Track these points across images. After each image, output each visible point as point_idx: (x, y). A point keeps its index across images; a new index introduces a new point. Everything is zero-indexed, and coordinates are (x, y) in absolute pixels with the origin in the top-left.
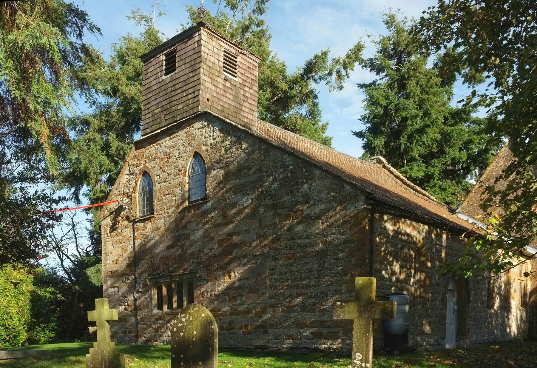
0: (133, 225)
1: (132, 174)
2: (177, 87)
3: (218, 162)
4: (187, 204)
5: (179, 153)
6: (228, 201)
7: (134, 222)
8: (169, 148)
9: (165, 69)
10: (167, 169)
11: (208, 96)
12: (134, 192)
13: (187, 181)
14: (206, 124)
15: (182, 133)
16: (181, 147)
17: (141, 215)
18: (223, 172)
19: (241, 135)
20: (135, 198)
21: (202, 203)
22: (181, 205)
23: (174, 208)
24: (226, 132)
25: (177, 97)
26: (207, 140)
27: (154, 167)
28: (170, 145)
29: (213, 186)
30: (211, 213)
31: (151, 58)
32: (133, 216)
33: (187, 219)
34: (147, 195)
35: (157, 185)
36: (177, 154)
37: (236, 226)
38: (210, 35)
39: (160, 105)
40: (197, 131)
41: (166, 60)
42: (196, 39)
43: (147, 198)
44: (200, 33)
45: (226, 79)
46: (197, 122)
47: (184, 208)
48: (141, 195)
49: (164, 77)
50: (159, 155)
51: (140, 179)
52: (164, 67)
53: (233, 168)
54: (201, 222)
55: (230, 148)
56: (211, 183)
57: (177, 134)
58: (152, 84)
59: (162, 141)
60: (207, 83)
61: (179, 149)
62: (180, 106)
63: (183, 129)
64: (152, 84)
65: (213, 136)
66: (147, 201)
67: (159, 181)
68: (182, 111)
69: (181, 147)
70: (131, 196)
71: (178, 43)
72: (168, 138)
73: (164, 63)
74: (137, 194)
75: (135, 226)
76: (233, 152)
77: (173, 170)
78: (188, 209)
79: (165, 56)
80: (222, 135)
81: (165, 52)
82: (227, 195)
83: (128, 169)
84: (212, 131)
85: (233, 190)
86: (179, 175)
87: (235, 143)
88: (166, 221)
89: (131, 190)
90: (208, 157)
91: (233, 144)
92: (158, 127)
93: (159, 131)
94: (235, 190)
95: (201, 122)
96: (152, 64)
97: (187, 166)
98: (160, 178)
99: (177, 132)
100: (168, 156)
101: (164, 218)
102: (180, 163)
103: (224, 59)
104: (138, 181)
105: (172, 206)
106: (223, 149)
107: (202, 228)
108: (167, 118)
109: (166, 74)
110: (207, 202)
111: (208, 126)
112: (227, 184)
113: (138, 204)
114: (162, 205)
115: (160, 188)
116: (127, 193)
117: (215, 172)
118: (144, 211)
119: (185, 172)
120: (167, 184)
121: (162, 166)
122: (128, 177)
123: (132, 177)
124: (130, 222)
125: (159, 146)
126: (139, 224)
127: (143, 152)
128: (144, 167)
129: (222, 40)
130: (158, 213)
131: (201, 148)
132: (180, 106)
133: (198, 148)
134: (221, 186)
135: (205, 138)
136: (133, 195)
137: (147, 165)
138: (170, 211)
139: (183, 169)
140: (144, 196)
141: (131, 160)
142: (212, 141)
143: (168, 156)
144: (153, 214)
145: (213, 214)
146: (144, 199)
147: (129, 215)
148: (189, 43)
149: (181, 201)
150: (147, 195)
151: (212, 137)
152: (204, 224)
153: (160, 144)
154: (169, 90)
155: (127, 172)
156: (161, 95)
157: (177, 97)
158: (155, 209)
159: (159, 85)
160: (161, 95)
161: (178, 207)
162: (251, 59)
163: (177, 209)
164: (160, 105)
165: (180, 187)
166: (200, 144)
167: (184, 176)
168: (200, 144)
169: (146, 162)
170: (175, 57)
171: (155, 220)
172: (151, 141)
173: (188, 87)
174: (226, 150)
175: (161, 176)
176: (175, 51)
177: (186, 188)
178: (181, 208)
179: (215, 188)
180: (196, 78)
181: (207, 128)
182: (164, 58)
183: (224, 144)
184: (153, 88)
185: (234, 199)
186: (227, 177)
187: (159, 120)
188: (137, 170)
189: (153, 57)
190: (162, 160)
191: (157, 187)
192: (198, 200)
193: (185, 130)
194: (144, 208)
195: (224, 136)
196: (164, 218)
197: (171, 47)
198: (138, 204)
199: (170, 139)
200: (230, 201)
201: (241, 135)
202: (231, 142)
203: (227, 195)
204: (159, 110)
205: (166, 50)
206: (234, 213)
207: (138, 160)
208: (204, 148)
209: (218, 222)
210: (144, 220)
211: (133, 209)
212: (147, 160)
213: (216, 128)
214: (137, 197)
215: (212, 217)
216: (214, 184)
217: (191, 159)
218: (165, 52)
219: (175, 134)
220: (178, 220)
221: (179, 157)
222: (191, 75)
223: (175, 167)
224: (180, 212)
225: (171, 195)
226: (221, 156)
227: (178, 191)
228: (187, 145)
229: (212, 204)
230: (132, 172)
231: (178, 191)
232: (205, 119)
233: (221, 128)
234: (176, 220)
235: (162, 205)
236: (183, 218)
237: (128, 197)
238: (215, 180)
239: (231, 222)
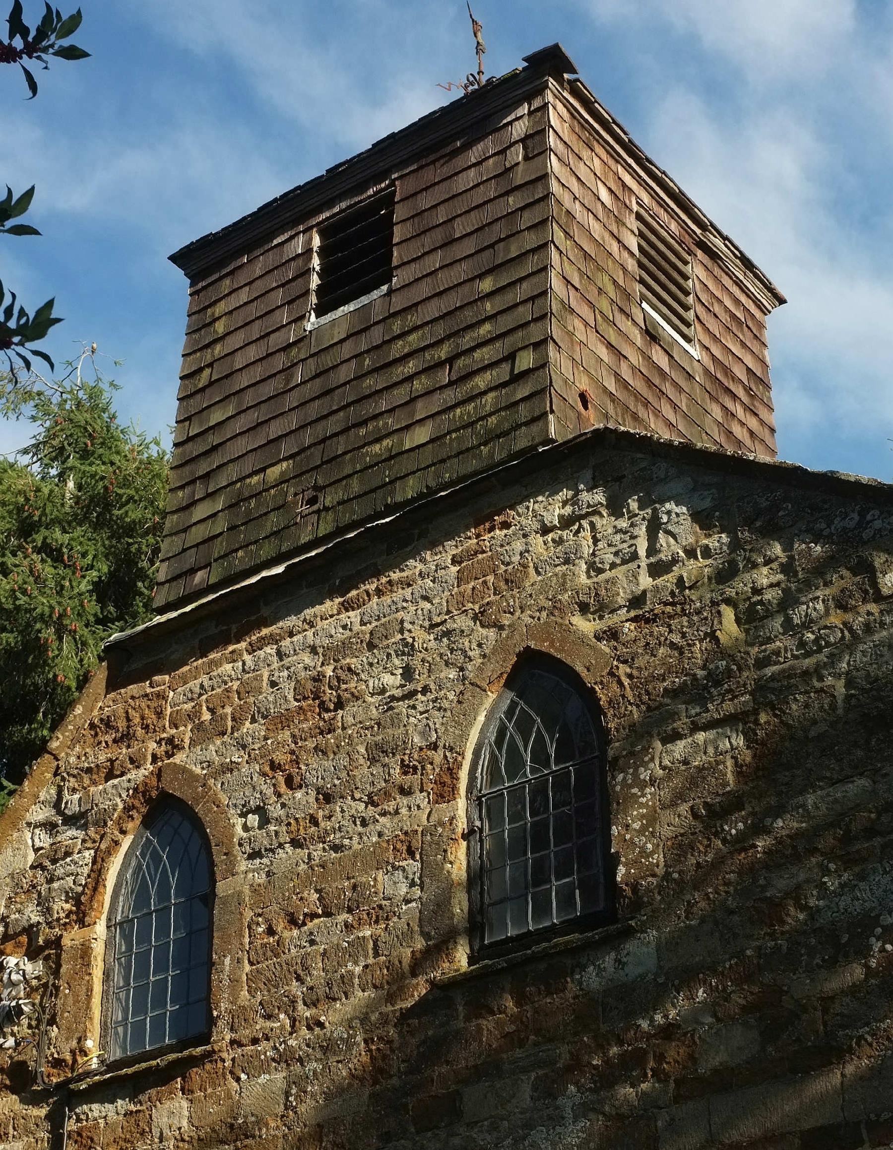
0: (55, 1120)
1: (71, 821)
2: (398, 349)
3: (695, 692)
4: (461, 958)
5: (408, 673)
6: (796, 916)
7: (65, 1097)
8: (335, 652)
9: (320, 290)
10: (316, 769)
11: (583, 384)
12: (81, 915)
13: (462, 825)
14: (599, 497)
15: (432, 573)
16: (421, 637)
17: (116, 1054)
18: (739, 741)
19: (862, 524)
20: (85, 952)
21: (573, 951)
22: (416, 968)
23: (360, 996)
24: (749, 523)
25: (401, 395)
26: (613, 581)
27: (231, 768)
28: (340, 635)
29: (667, 832)
30: (656, 1002)
31: (238, 254)
32: (58, 1063)
33: (463, 1058)
34: (163, 930)
35: (243, 865)
36: (392, 681)
37: (876, 1073)
38: (584, 125)
39: (285, 449)
40: (537, 541)
41: (322, 252)
42: (519, 129)
43: (162, 951)
44: (537, 103)
45: (652, 335)
46: (527, 498)
47: (442, 991)
48: (127, 938)
49: (312, 322)
50: (267, 696)
51: (126, 842)
52: (315, 281)
53: (814, 712)
54: (576, 1065)
55: (788, 601)
56: (652, 819)
57: (395, 576)
58: (239, 361)
59: (291, 621)
60: (578, 323)
61: (408, 649)
62: (421, 435)
63: (434, 545)
64: (239, 361)
65: (652, 551)
66: (161, 967)
67: (262, 839)
68: (427, 456)
69: (421, 637)
70: (56, 943)
71: (405, 163)
72: (330, 606)
73: (316, 262)
74: (100, 929)
75: (71, 1125)
76: (808, 624)
77: (363, 771)
78: (474, 989)
79: (321, 234)
80: (718, 541)
81: (323, 216)
82: (781, 883)
83: (48, 793)
84: (642, 531)
85: (827, 841)
86: (405, 792)
87: (821, 570)
88: (298, 1082)
89: (61, 907)
90: (623, 669)
91: (799, 581)
92: (267, 551)
93: (279, 569)
94: (847, 839)
95: (566, 494)
96: (242, 278)
97: (464, 737)
98: (265, 821)
99: (397, 565)
100: (323, 699)
101: (285, 1058)
102: (413, 725)
103: (640, 247)
104: (109, 852)
105: (346, 981)
106: (728, 613)
107: (583, 1110)
108: (329, 500)
109: (320, 311)
110: (628, 933)
111: (616, 508)
112: (778, 811)
113: (98, 988)
114: (272, 983)
115: (261, 879)
116: (30, 930)
117: (680, 748)
118: (139, 1028)
119: (452, 772)
120: (318, 852)
121: (280, 757)
122: (43, 840)
123: (69, 835)
124: (34, 1100)
125: (270, 650)
126: (96, 1110)
127: (161, 696)
128: (159, 774)
129: (630, 161)
130: (245, 1033)
131: (568, 629)
132: (421, 435)
133: (545, 631)
134: (734, 828)
135: (594, 568)
136: (71, 938)
137: (179, 758)
138: (335, 1016)
139: (438, 757)
140: (144, 937)
141: (75, 741)
142: (646, 581)
143: (329, 695)
144: (206, 1039)
145: (675, 1009)
146: (143, 959)
147: (30, 1055)
148: (473, 155)
149: (420, 944)
150: (163, 930)
151: (644, 562)
152: (608, 1079)
153: (274, 639)
154: (345, 373)
155: (39, 814)
156: (292, 400)
157: (401, 395)
158: (223, 1007)
159: (280, 361)
160: (292, 400)
161: (394, 984)
162: (738, 283)
163: (391, 998)
164: (285, 449)
165: (413, 866)
166: (557, 608)
167: (444, 792)
168: (557, 608)
169: (174, 746)
170: (388, 224)
171: (217, 1078)
172: (213, 630)
173: (467, 341)
174: (751, 617)
175: (275, 811)
176: (387, 200)
177: (458, 862)
178: (420, 988)
179: (681, 847)
180: (523, 291)
181: (605, 523)
182: (316, 242)
183: (740, 586)
184: (244, 380)
185: (844, 902)
186: (773, 772)
187: (274, 521)
188: (112, 795)
189: (248, 248)
190: (284, 720)
191: (240, 879)
192: (552, 931)
193: (451, 549)
194: (140, 1008)
195: (735, 545)
196: (285, 1058)
197: (362, 187)
198: (98, 988)
199: (347, 607)
200: (813, 913)
201: (862, 524)
202: (787, 569)
203: (781, 883)
204: (274, 473)
205: (330, 204)
206: (853, 990)
207: (126, 738)
208: (585, 626)
209: (715, 1059)
210: (130, 1080)
211: (65, 1018)
212: (186, 733)
213: (676, 513)
214: (98, 948)
215: (668, 1032)
216: (675, 821)
217: (487, 708)
218: (323, 216)
219: (377, 574)
220: (396, 1064)
221: (412, 694)
222: (487, 285)
223: (377, 753)
224: (406, 1015)
225: (344, 916)
226: (719, 651)
227: (395, 885)
228: (463, 622)
229: (665, 948)
230: (73, 808)
231: (395, 885)
232: (588, 474)
233: (707, 504)
234: (378, 1070)
235: (272, 983)
236: (435, 1049)
237: (32, 954)
238: (679, 797)
239: (832, 1053)
